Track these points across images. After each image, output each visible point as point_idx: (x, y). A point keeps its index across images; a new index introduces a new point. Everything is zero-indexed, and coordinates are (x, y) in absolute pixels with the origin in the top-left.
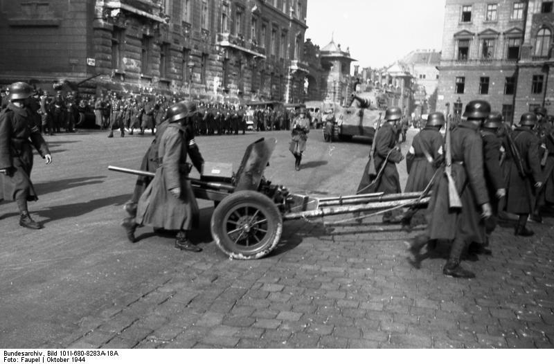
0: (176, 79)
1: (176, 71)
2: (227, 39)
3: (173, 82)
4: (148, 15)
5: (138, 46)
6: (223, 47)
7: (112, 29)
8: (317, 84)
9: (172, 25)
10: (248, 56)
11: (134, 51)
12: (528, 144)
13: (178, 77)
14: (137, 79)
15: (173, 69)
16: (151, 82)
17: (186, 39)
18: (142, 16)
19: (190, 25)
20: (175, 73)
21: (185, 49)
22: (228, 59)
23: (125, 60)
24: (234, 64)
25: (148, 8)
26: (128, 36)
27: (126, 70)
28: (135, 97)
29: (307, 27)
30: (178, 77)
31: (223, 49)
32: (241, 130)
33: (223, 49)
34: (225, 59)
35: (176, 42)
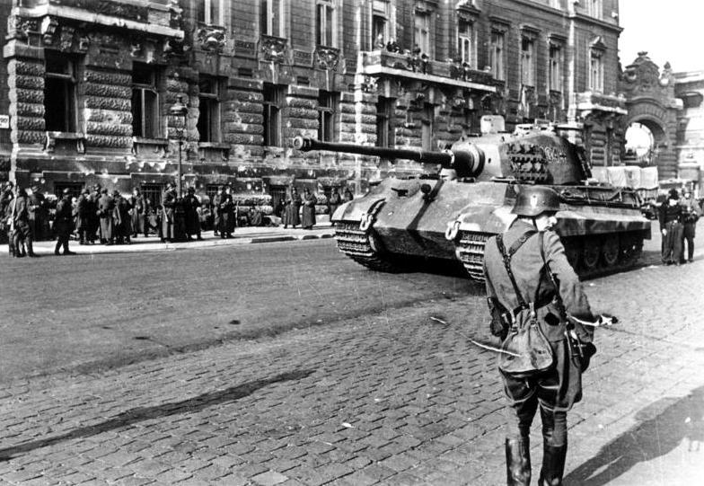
0: (246, 143)
1: (245, 127)
2: (379, 60)
3: (240, 149)
4: (141, 26)
5: (125, 85)
6: (374, 75)
7: (317, 95)
8: (668, 135)
9: (232, 42)
10: (449, 90)
11: (115, 96)
12: (367, 248)
13: (251, 138)
14: (123, 147)
15: (239, 123)
16: (167, 151)
17: (272, 67)
18: (134, 31)
19: (339, 51)
20: (243, 132)
21: (322, 92)
22: (392, 100)
23: (88, 113)
24: (408, 106)
25: (141, 13)
26: (90, 67)
27: (92, 132)
28: (115, 181)
29: (622, 29)
30: (251, 138)
31: (373, 80)
32: (194, 234)
33: (373, 80)
34: (382, 99)
35: (245, 72)
